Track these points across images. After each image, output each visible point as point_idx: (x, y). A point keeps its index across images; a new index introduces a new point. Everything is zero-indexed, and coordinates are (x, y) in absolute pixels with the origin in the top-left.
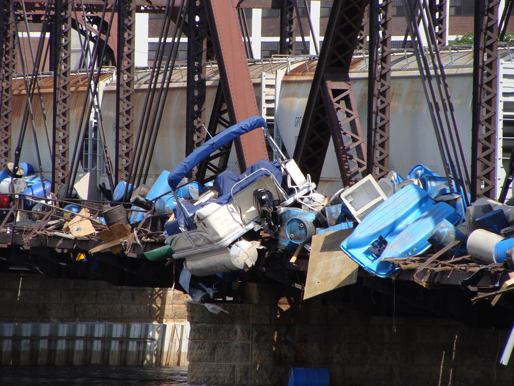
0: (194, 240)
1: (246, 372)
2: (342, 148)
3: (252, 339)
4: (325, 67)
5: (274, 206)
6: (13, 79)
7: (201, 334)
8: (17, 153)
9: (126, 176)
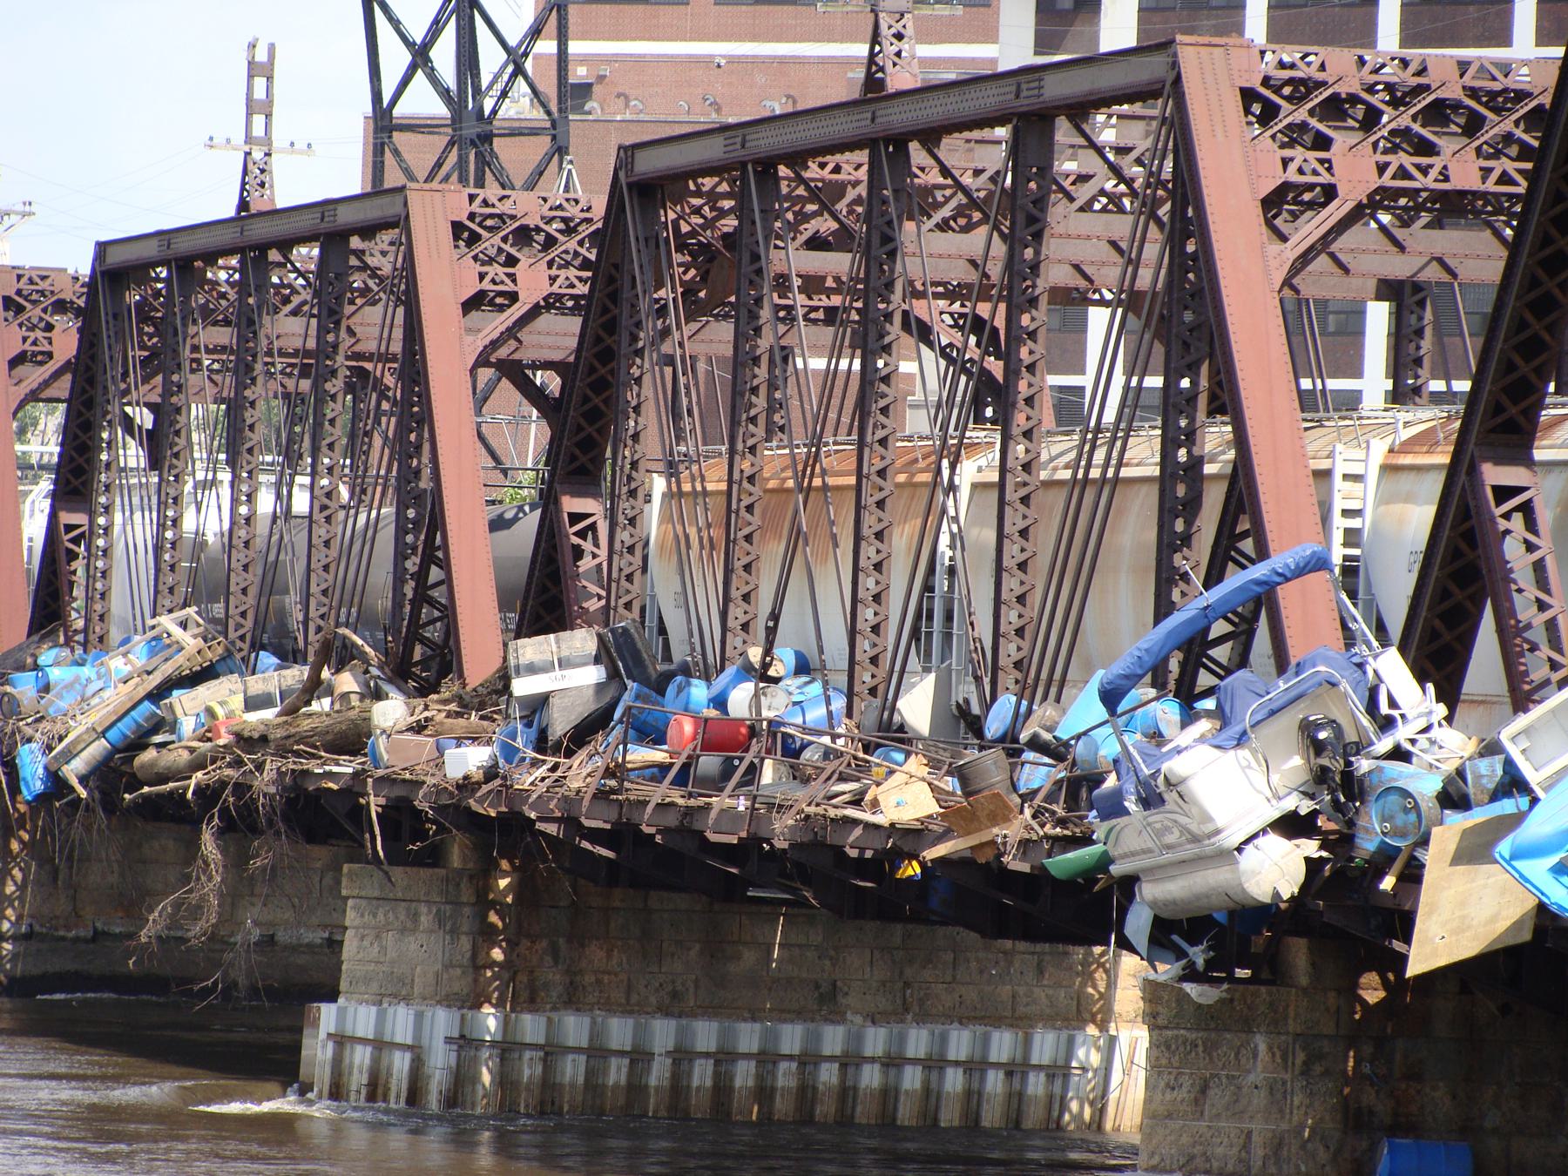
0: (1160, 834)
1: (1277, 1146)
2: (1513, 622)
3: (1293, 1071)
4: (1479, 432)
5: (1346, 755)
6: (766, 452)
7: (1174, 1053)
8: (771, 624)
9: (1017, 682)
